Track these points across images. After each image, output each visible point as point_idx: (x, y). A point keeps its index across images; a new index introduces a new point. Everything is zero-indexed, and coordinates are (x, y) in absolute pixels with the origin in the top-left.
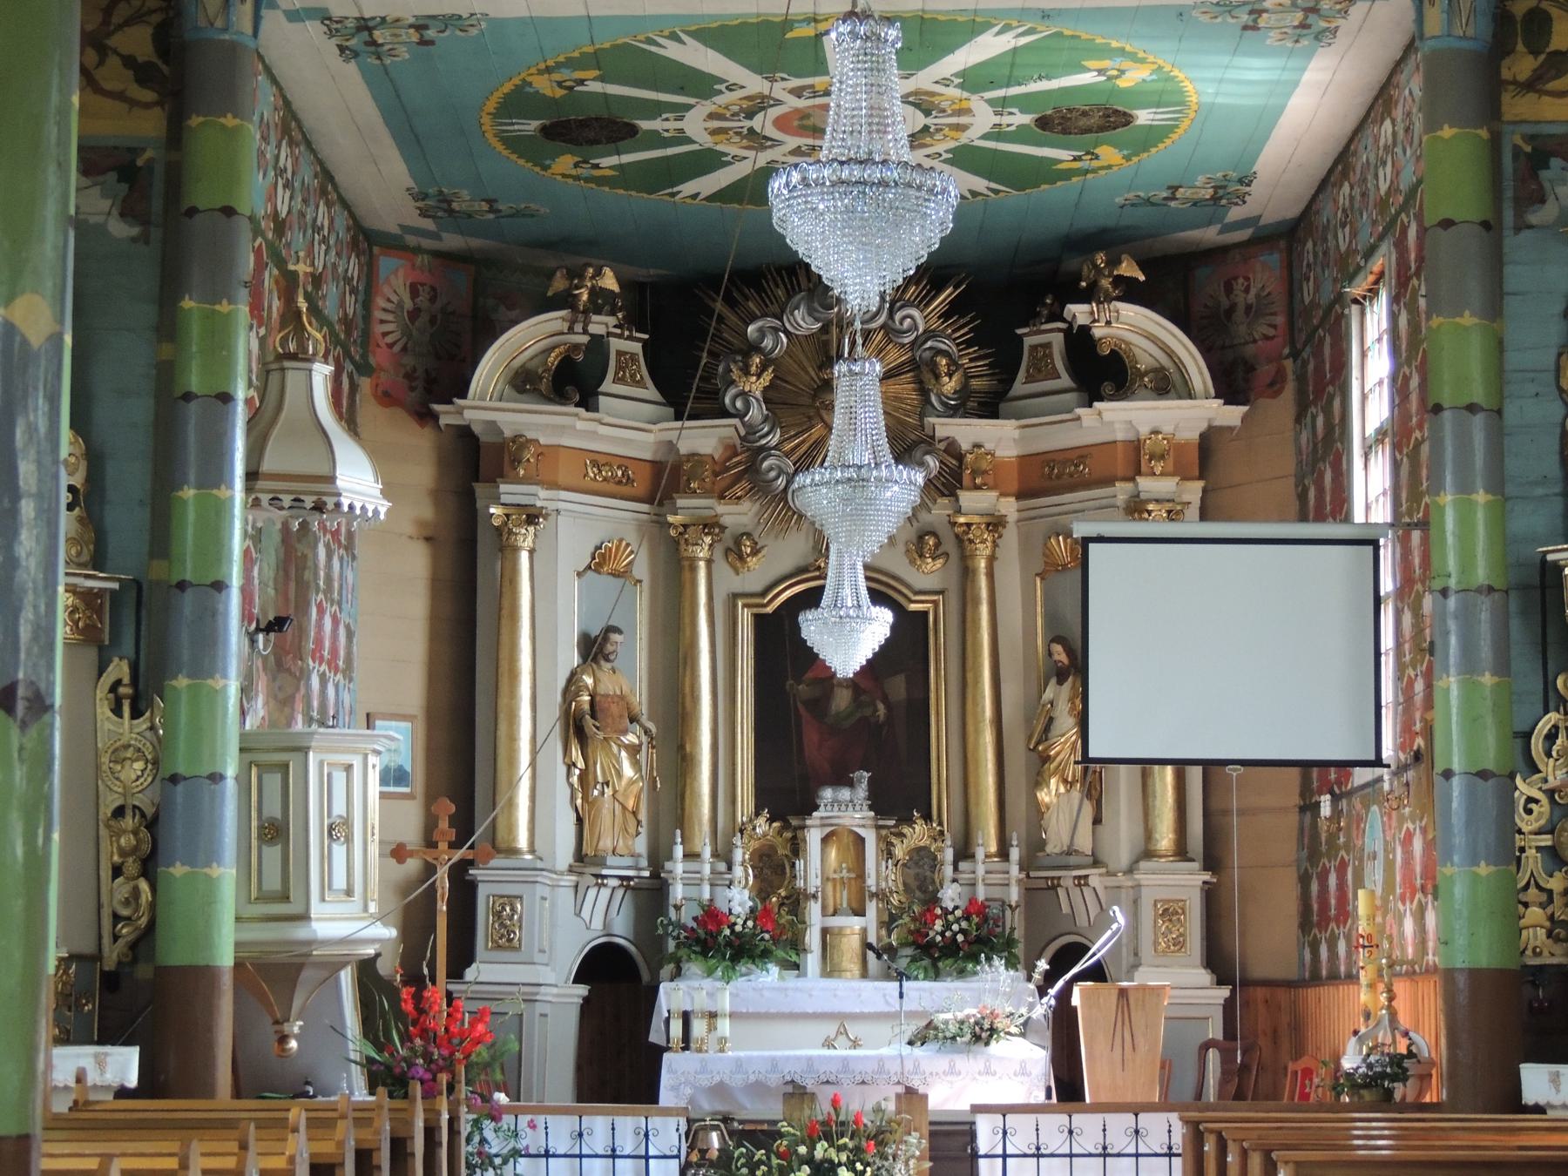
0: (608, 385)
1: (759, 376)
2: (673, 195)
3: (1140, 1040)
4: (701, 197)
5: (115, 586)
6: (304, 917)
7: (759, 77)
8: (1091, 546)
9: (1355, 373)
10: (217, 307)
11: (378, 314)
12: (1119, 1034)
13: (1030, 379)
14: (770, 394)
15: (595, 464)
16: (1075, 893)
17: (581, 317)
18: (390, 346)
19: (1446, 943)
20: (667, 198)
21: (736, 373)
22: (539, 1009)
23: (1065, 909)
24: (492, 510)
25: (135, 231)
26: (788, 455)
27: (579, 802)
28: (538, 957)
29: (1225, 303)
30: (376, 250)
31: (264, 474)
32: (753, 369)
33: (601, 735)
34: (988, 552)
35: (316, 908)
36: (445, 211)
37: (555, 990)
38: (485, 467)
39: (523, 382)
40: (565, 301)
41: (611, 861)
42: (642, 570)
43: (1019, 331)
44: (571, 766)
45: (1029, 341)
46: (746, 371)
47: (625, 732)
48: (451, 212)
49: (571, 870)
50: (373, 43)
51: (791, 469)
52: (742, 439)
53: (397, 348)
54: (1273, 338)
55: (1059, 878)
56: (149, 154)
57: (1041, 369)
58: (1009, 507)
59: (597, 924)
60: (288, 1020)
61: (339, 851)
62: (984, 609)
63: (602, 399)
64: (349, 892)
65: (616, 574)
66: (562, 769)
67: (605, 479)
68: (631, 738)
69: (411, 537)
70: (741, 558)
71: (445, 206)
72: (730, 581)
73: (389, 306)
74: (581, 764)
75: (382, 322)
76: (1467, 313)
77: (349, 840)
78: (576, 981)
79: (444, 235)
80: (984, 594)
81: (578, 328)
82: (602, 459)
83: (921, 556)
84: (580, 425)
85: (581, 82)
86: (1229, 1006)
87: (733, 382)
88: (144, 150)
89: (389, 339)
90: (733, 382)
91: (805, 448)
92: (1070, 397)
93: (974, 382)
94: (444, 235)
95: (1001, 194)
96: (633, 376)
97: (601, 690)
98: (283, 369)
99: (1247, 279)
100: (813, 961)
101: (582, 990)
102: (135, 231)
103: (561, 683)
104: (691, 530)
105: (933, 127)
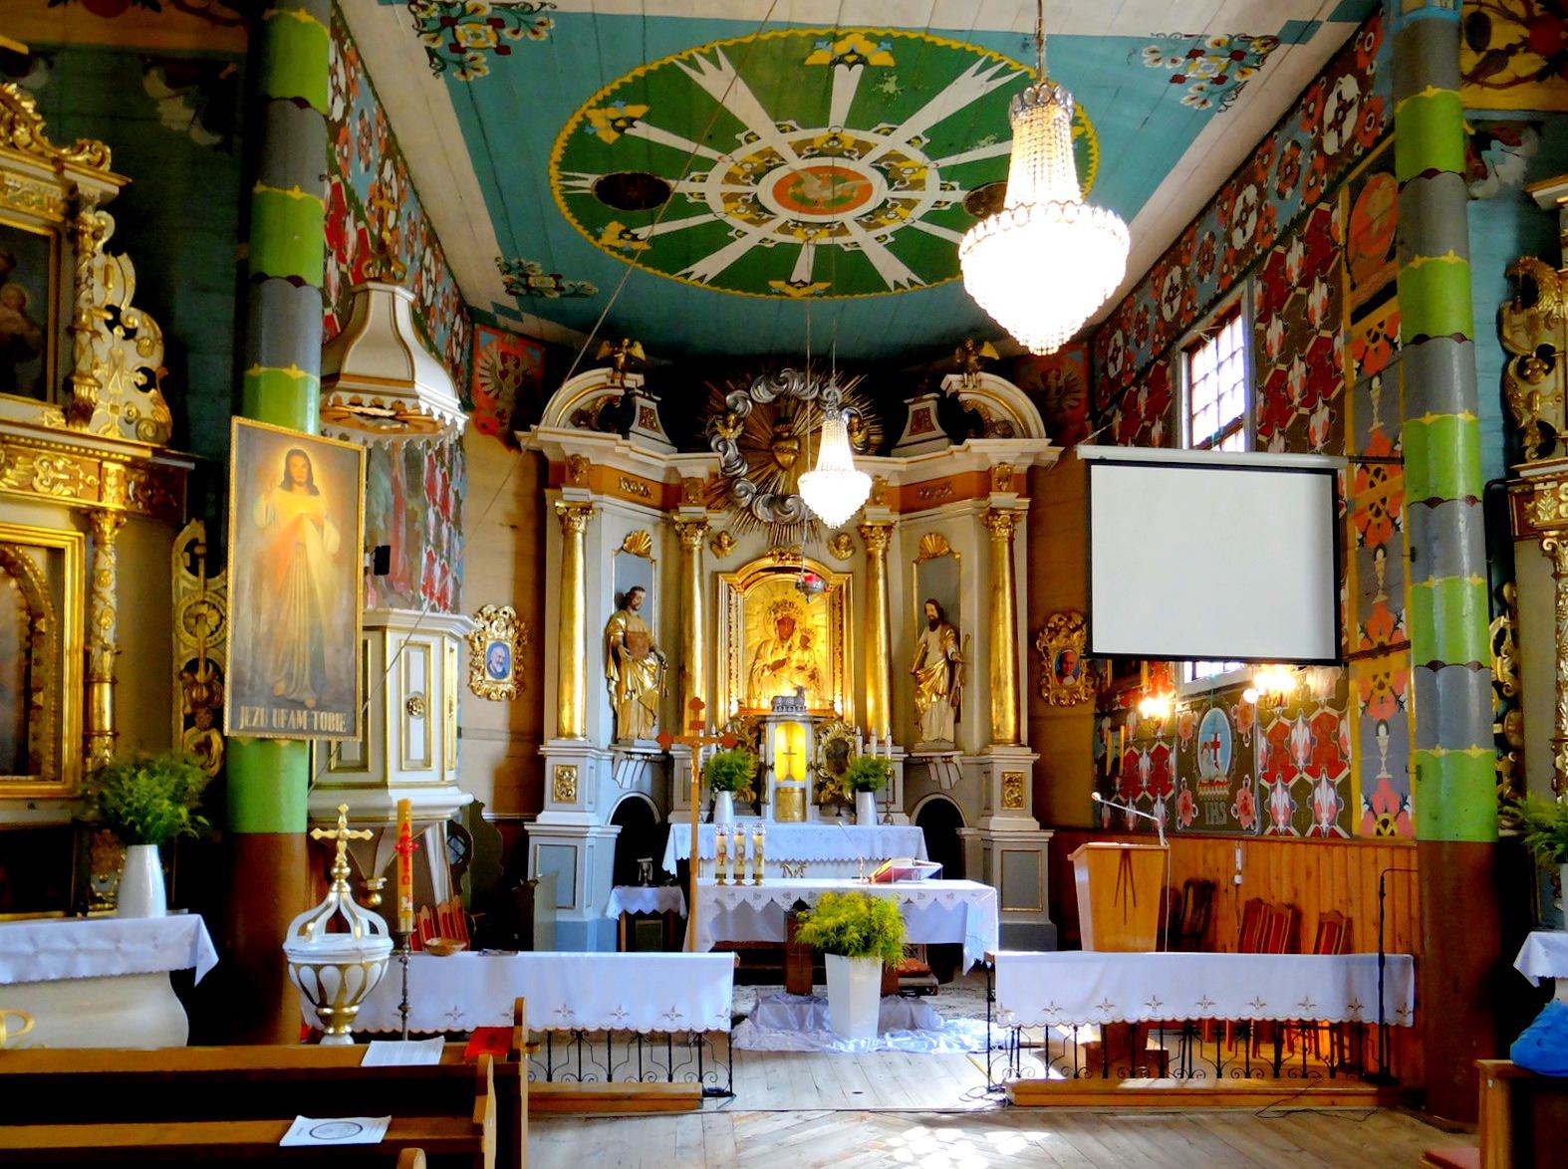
0: (635, 427)
1: (734, 428)
2: (687, 276)
3: (1140, 898)
4: (707, 279)
5: (191, 466)
6: (383, 785)
7: (773, 124)
8: (1095, 468)
9: (1185, 401)
10: (289, 193)
11: (478, 370)
12: (1121, 889)
13: (913, 432)
14: (743, 442)
15: (626, 480)
16: (942, 768)
17: (619, 375)
18: (487, 393)
19: (1436, 818)
20: (682, 279)
21: (720, 428)
22: (588, 842)
23: (934, 777)
24: (557, 504)
25: (216, 139)
26: (753, 481)
27: (615, 703)
28: (587, 807)
29: (1041, 386)
30: (476, 325)
31: (346, 375)
32: (731, 423)
33: (630, 658)
34: (883, 545)
35: (393, 776)
36: (524, 286)
37: (599, 830)
38: (551, 478)
39: (580, 419)
40: (609, 362)
41: (637, 742)
42: (656, 553)
43: (906, 402)
44: (609, 679)
45: (912, 408)
46: (726, 426)
47: (646, 657)
48: (528, 287)
49: (609, 748)
50: (455, 47)
51: (755, 490)
52: (723, 469)
53: (492, 395)
54: (1077, 407)
55: (931, 757)
56: (232, 68)
57: (921, 422)
58: (895, 517)
59: (627, 785)
60: (372, 878)
61: (416, 724)
62: (881, 582)
63: (631, 434)
64: (427, 763)
65: (638, 554)
66: (604, 682)
67: (633, 491)
68: (648, 661)
69: (501, 525)
70: (721, 547)
71: (523, 281)
72: (712, 562)
73: (486, 366)
74: (617, 678)
75: (481, 376)
76: (1451, 252)
77: (426, 716)
78: (613, 823)
79: (525, 316)
80: (881, 572)
81: (617, 383)
82: (631, 478)
83: (838, 548)
84: (618, 449)
85: (631, 121)
86: (1052, 843)
87: (717, 432)
88: (225, 64)
89: (486, 389)
90: (717, 432)
91: (763, 477)
92: (946, 440)
93: (872, 438)
94: (525, 316)
95: (916, 287)
96: (651, 423)
97: (630, 629)
98: (367, 291)
99: (1058, 370)
100: (768, 810)
101: (618, 829)
102: (216, 139)
103: (604, 625)
104: (689, 526)
105: (891, 202)
